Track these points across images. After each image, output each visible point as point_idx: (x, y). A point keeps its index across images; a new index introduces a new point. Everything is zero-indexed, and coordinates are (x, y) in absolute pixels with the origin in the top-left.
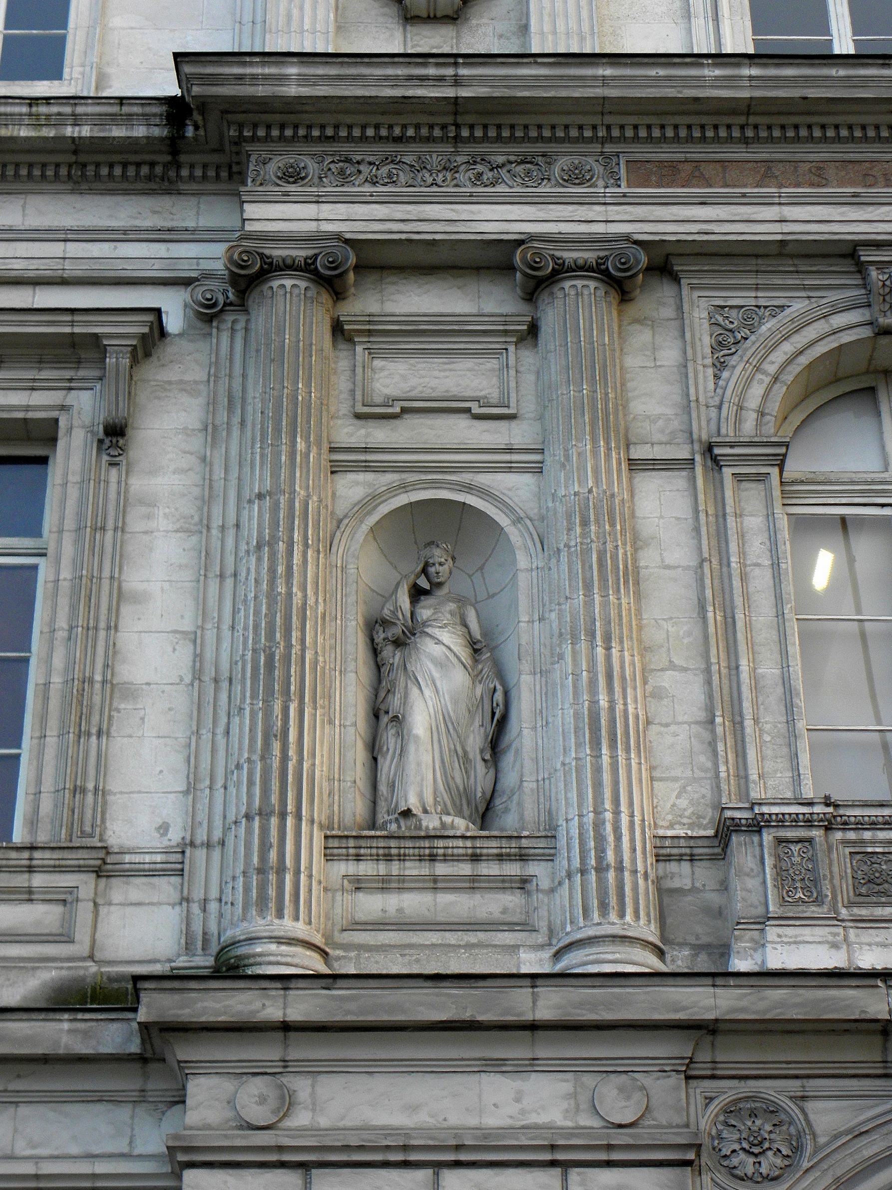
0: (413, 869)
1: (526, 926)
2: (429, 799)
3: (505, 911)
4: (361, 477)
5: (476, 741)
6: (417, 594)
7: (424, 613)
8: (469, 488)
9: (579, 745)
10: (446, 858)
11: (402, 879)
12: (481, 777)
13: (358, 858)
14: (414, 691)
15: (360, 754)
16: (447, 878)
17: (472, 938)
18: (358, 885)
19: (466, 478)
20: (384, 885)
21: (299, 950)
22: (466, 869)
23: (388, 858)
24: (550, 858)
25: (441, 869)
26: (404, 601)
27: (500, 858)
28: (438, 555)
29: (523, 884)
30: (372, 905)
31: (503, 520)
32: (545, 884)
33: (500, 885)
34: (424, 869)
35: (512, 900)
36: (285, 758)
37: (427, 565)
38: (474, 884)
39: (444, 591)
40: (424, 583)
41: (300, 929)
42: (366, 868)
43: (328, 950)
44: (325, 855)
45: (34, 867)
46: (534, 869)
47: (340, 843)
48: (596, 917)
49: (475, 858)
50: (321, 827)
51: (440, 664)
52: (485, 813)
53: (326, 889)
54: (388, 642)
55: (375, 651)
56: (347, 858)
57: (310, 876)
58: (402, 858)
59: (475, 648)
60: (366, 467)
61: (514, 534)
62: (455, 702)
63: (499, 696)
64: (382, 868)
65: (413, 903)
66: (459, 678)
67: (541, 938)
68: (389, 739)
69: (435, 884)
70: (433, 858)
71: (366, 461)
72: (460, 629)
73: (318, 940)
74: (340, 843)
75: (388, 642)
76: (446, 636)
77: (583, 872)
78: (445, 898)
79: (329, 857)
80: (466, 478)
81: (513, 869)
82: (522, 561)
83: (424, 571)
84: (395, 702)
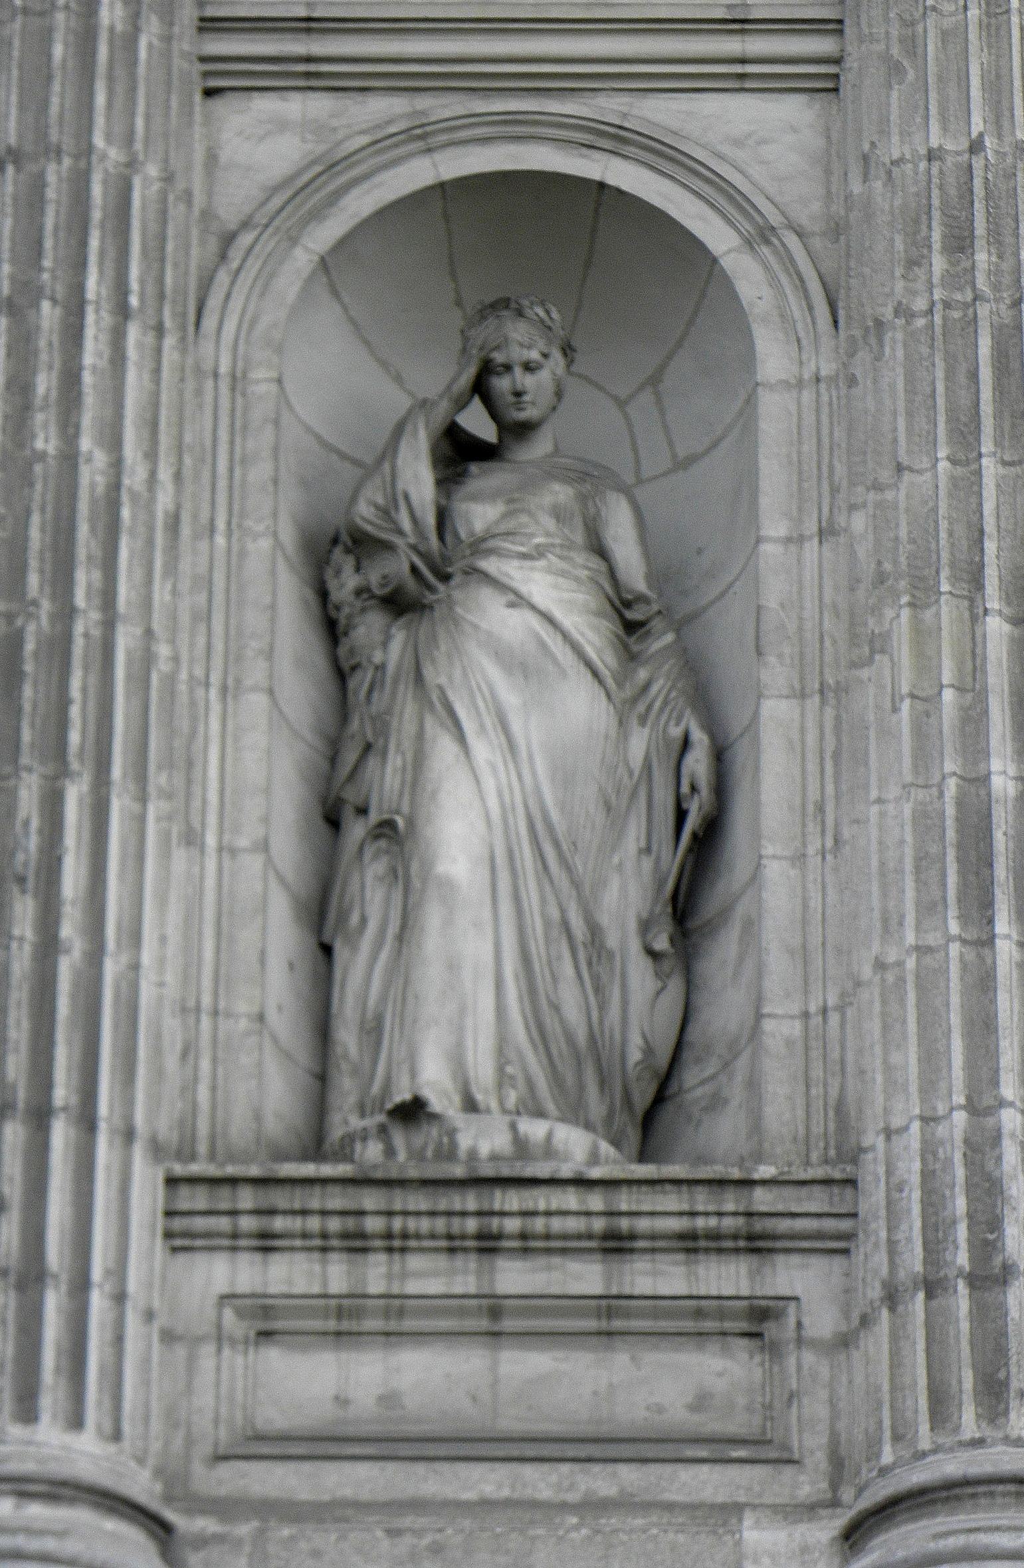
0: (430, 1276)
1: (764, 1448)
2: (483, 1070)
3: (701, 1402)
4: (294, 106)
5: (627, 893)
6: (459, 454)
7: (479, 514)
8: (617, 139)
9: (930, 908)
10: (528, 1245)
11: (396, 1304)
12: (641, 1005)
13: (266, 1243)
14: (444, 748)
15: (280, 936)
16: (534, 1304)
17: (601, 1482)
18: (266, 1322)
19: (608, 107)
20: (345, 1323)
21: (82, 1516)
22: (586, 1276)
23: (356, 1243)
24: (839, 1245)
25: (514, 1277)
26: (418, 476)
27: (691, 1244)
28: (520, 340)
29: (758, 1321)
30: (308, 1382)
31: (716, 234)
32: (823, 1321)
33: (688, 1325)
34: (461, 1277)
35: (720, 1373)
36: (48, 946)
37: (487, 370)
38: (610, 1322)
39: (539, 447)
40: (478, 423)
41: (85, 1453)
42: (289, 1274)
43: (170, 1515)
44: (168, 1235)
45: (274, 1236)
46: (790, 1276)
47: (212, 1199)
48: (969, 1421)
49: (615, 1244)
50: (157, 1150)
51: (518, 665)
52: (652, 1111)
53: (168, 1337)
54: (372, 593)
55: (332, 629)
56: (233, 1242)
57: (120, 1298)
58: (397, 1244)
59: (629, 620)
60: (310, 77)
61: (749, 277)
62: (565, 777)
63: (698, 763)
64: (337, 1274)
65: (429, 1377)
66: (581, 707)
67: (807, 1484)
68: (370, 892)
69: (494, 1322)
70: (488, 1244)
71: (309, 59)
72: (584, 562)
73: (141, 1486)
74: (212, 1199)
75: (372, 593)
76: (541, 584)
77: (933, 1287)
78: (523, 1365)
79: (179, 1239)
80: (608, 107)
81: (726, 1277)
82: (773, 358)
83: (480, 388)
84: (386, 781)
